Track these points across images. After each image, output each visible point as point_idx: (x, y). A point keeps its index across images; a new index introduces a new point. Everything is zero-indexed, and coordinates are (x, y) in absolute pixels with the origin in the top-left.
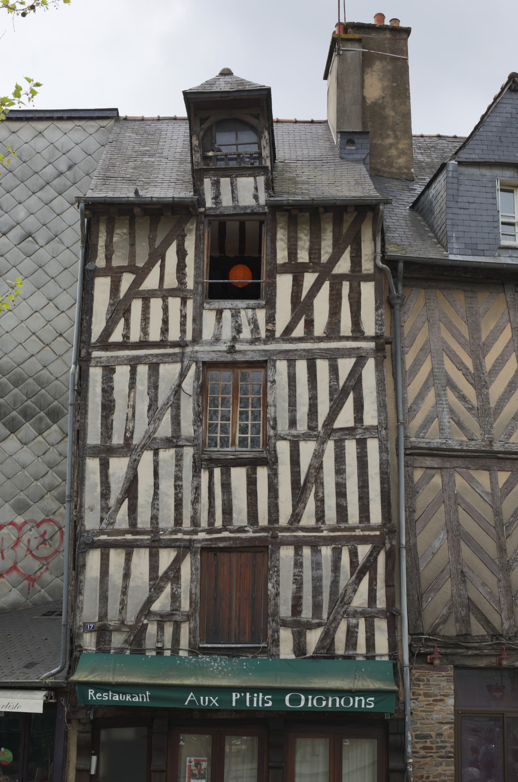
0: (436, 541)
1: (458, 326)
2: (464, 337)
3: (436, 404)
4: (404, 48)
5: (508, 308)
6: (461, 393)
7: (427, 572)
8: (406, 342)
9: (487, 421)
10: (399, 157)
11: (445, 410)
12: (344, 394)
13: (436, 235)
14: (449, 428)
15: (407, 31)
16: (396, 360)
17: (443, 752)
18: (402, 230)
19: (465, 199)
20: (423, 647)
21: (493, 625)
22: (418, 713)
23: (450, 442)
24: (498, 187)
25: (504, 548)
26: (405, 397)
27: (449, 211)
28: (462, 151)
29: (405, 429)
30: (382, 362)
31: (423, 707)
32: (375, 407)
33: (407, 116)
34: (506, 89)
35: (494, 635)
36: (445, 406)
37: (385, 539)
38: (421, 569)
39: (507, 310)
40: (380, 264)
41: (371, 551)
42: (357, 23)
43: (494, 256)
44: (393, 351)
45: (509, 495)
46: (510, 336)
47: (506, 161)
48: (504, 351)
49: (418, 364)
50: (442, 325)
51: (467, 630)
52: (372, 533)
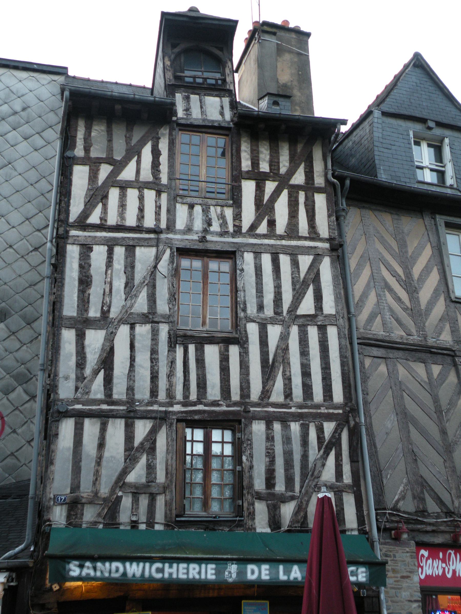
32: (332, 298)
37: (348, 417)
41: (336, 428)
46: (431, 253)
48: (427, 264)
50: (376, 239)
52: (336, 411)
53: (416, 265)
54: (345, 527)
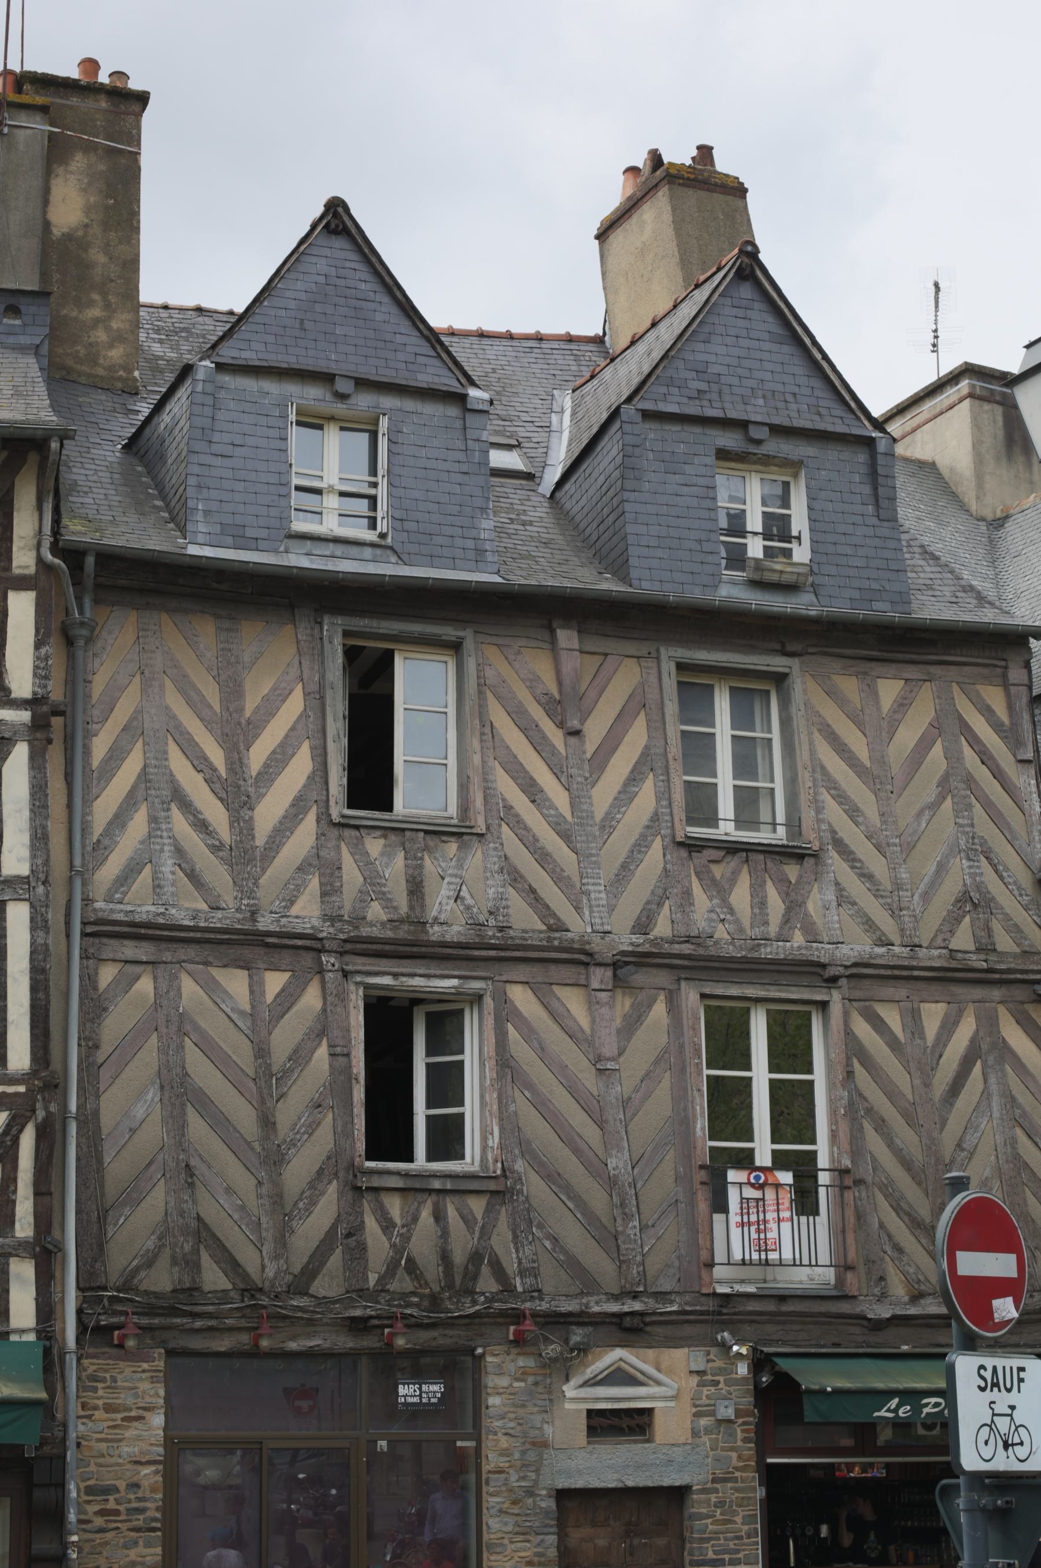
0: (139, 1105)
1: (199, 686)
2: (210, 707)
3: (150, 836)
4: (134, 132)
5: (300, 655)
6: (200, 817)
7: (118, 1168)
8: (96, 712)
9: (248, 873)
10: (111, 346)
11: (166, 848)
13: (167, 505)
14: (172, 885)
15: (143, 98)
16: (73, 748)
17: (140, 1521)
18: (102, 491)
19: (226, 438)
20: (105, 1313)
21: (244, 1271)
22: (93, 1443)
23: (173, 911)
24: (293, 417)
25: (273, 1120)
26: (87, 822)
27: (194, 458)
28: (225, 344)
29: (84, 884)
30: (44, 751)
31: (102, 1432)
32: (26, 838)
33: (131, 266)
34: (319, 228)
36: (166, 841)
37: (35, 1100)
38: (107, 1160)
39: (297, 657)
40: (49, 557)
41: (8, 1125)
42: (43, 74)
43: (276, 551)
44: (69, 729)
46: (301, 708)
47: (311, 368)
48: (287, 736)
49: (116, 756)
50: (168, 683)
51: (194, 1280)
53: (257, 742)
54: (8, 1326)
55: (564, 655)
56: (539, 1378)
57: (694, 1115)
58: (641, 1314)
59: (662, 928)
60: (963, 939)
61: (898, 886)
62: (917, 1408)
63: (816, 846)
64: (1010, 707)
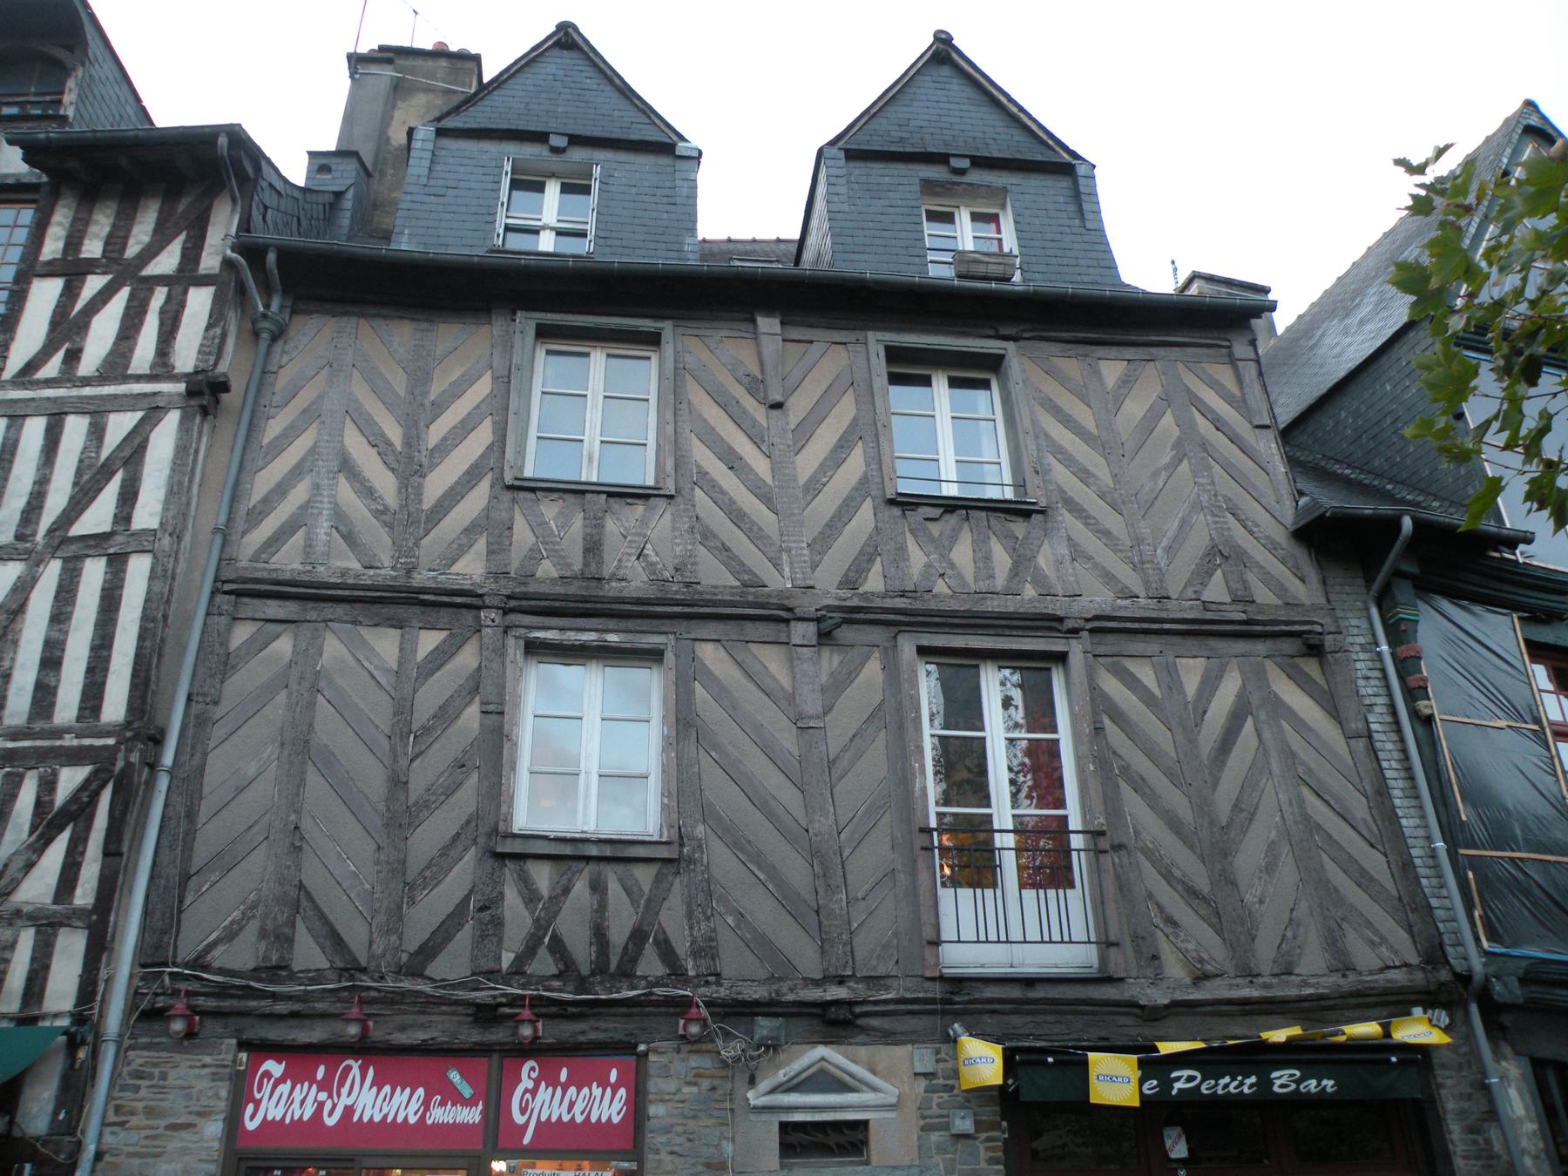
2: (394, 391)
8: (277, 399)
12: (106, 472)
22: (122, 1159)
32: (161, 494)
35: (346, 970)
45: (438, 674)
49: (290, 435)
52: (98, 742)
55: (764, 339)
56: (716, 1082)
57: (913, 774)
58: (850, 1004)
59: (874, 582)
60: (1216, 590)
61: (1138, 541)
62: (1167, 1084)
63: (1043, 503)
64: (1240, 380)
